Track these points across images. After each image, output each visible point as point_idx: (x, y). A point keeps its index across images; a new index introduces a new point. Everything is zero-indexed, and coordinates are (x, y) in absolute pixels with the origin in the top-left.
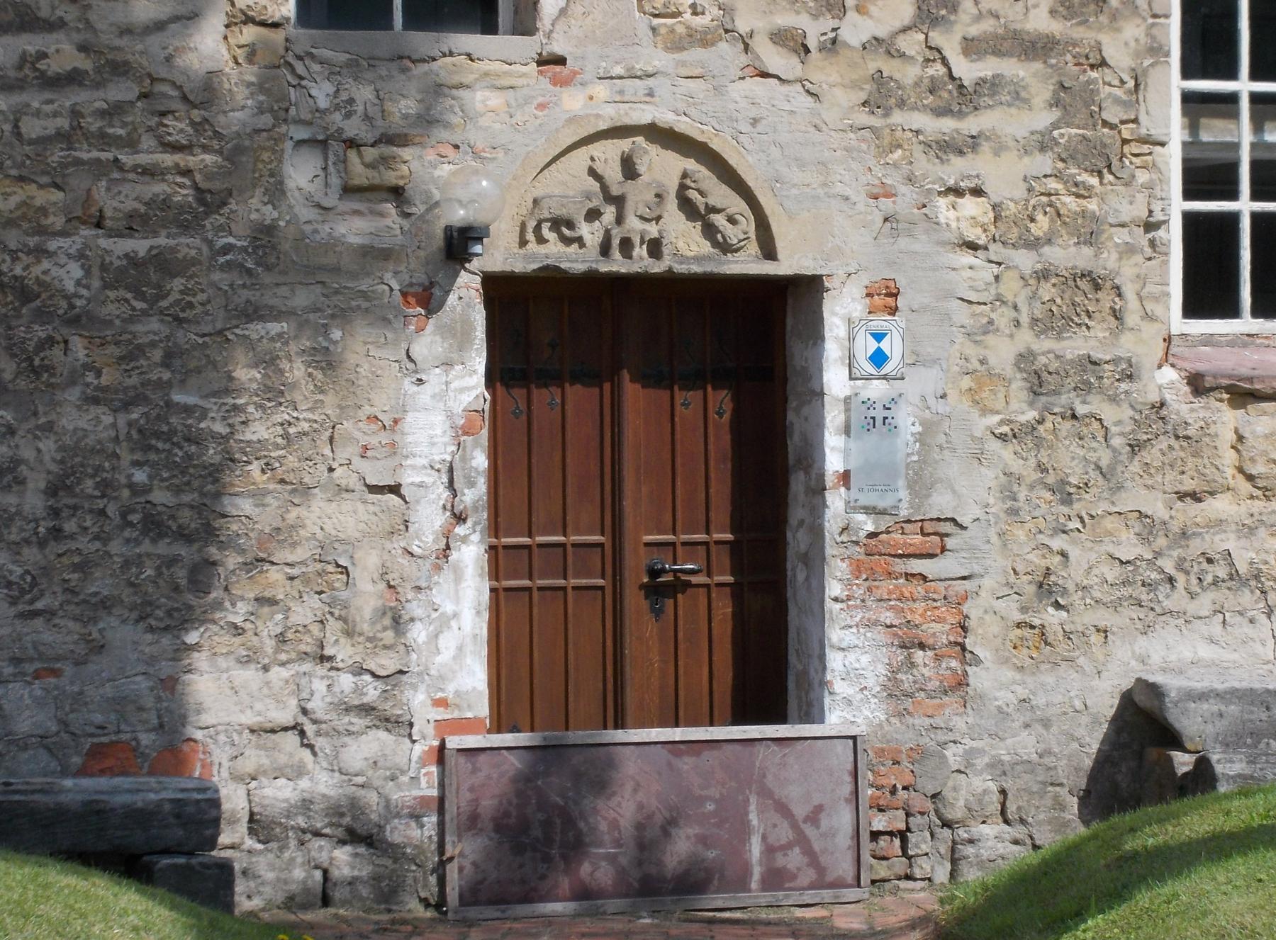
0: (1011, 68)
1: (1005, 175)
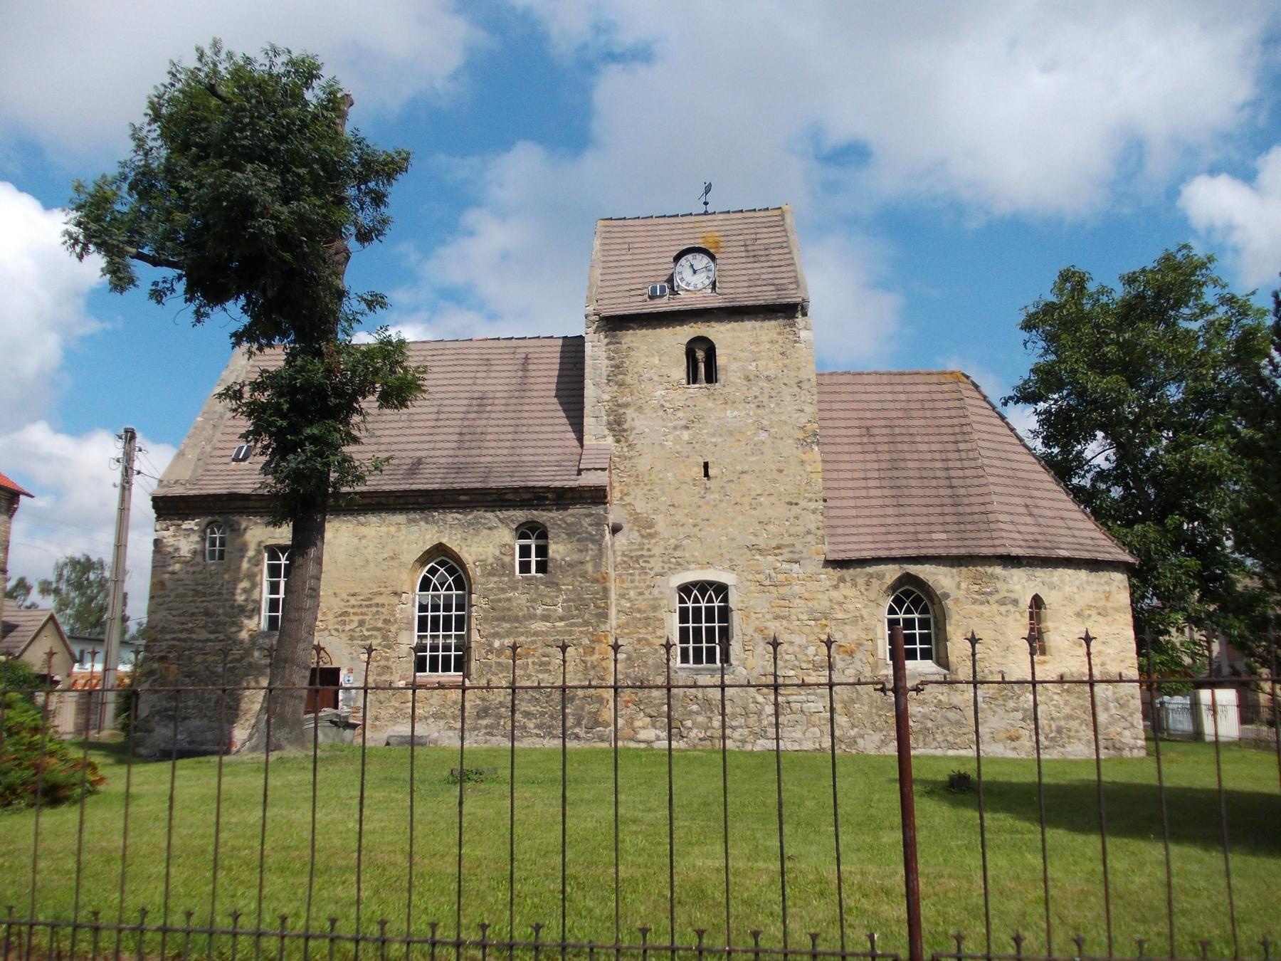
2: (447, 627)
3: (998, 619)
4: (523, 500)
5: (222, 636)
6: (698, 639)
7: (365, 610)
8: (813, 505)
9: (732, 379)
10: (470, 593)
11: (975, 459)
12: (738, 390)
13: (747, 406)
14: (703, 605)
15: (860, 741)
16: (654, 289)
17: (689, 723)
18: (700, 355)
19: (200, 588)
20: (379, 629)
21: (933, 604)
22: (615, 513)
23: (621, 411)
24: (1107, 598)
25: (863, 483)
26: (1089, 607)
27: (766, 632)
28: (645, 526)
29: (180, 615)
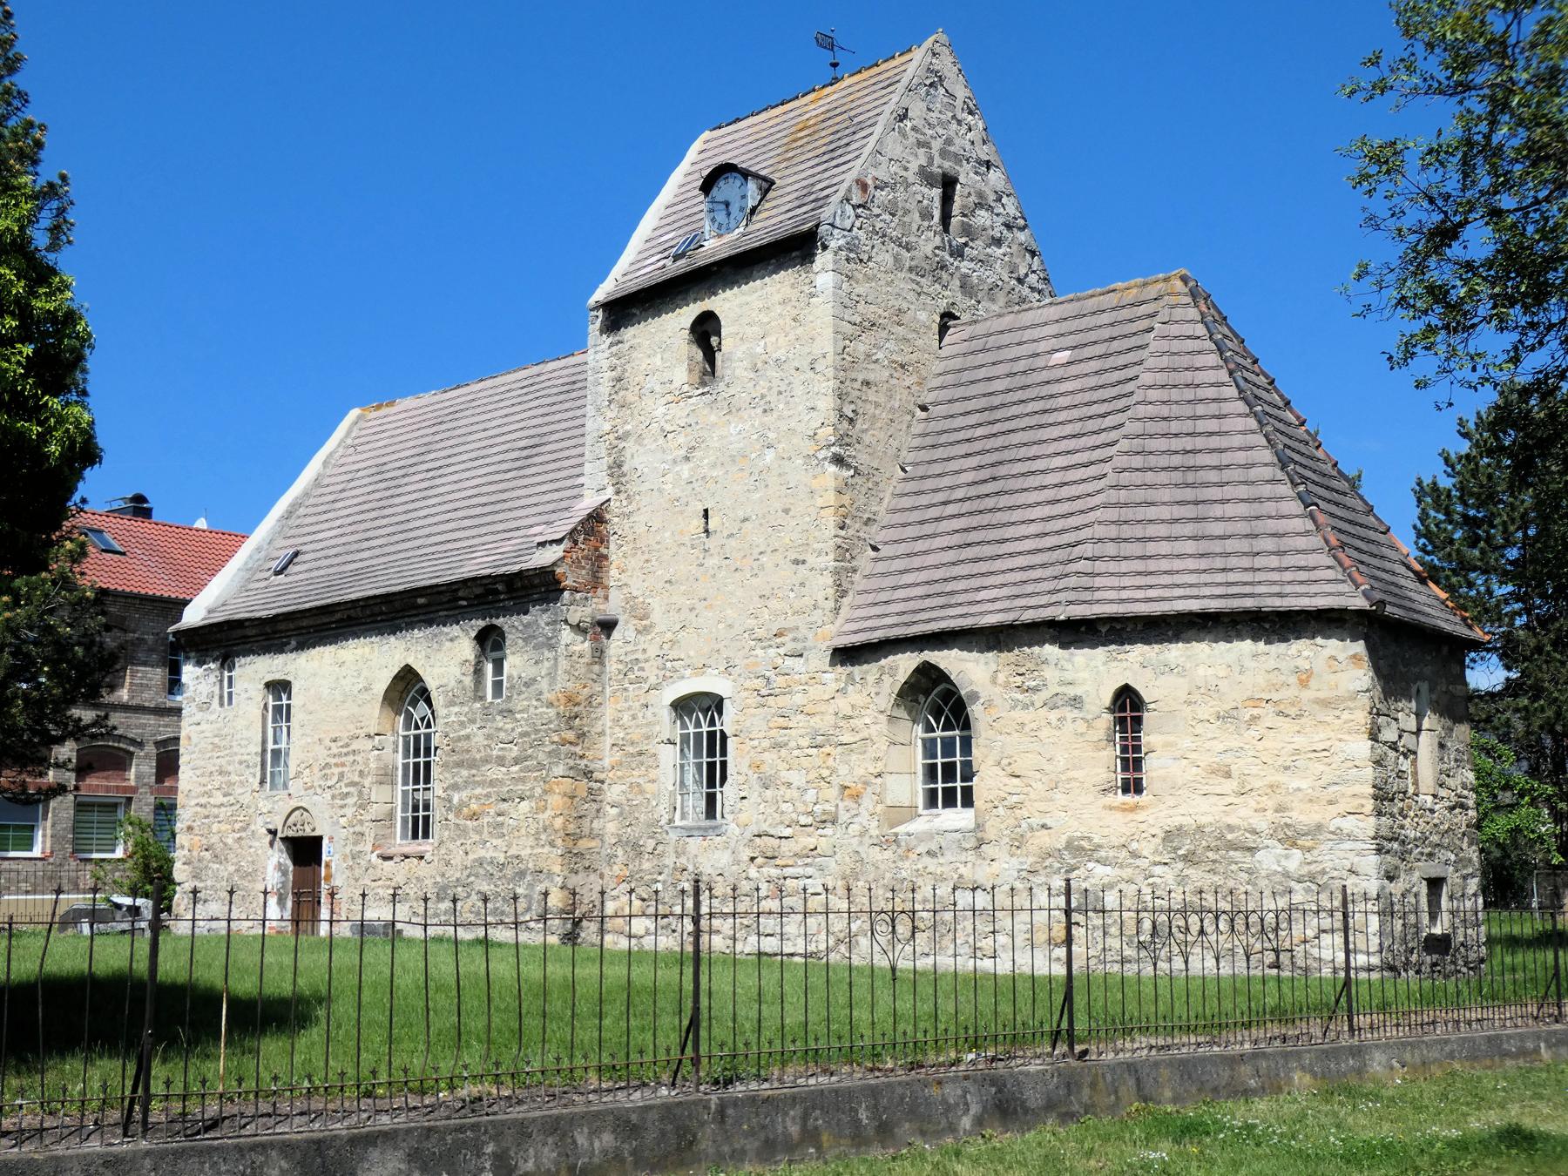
13: (753, 412)
24: (1304, 684)
26: (1255, 701)
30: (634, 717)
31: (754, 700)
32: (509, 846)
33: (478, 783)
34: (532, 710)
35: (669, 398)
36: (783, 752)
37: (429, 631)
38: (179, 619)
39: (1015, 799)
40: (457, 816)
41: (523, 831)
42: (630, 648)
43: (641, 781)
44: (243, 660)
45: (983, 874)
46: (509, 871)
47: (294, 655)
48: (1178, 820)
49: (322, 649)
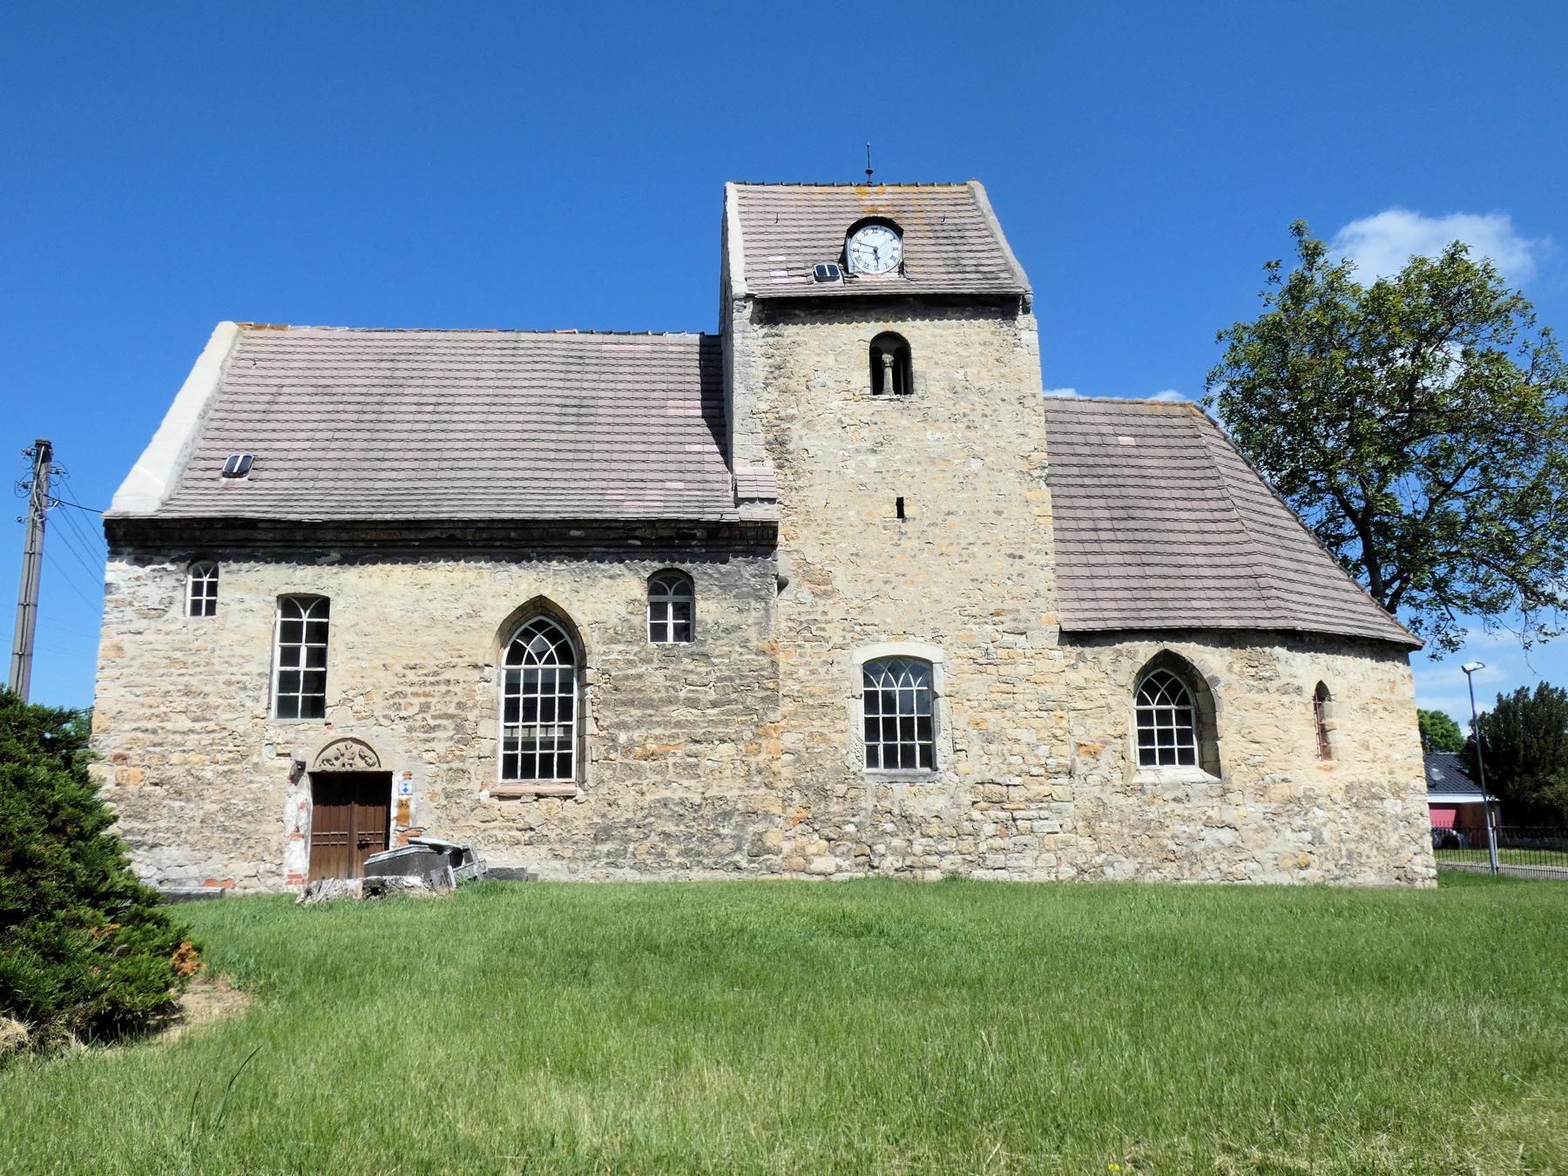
0: (444, 722)
1: (441, 747)
2: (548, 715)
3: (1279, 711)
4: (661, 538)
5: (211, 726)
6: (889, 734)
7: (428, 689)
8: (1042, 559)
9: (932, 389)
10: (583, 667)
11: (1229, 510)
12: (942, 405)
14: (897, 689)
15: (1109, 871)
16: (821, 269)
17: (881, 848)
18: (887, 358)
19: (178, 655)
20: (451, 717)
21: (1195, 690)
22: (783, 562)
23: (785, 425)
25: (1093, 536)
27: (983, 726)
28: (822, 584)
29: (147, 695)
30: (813, 672)
31: (969, 667)
32: (708, 787)
33: (659, 724)
34: (735, 656)
35: (849, 396)
36: (1008, 713)
37: (574, 565)
38: (109, 505)
39: (1257, 759)
40: (625, 755)
41: (727, 773)
42: (803, 609)
43: (825, 731)
44: (234, 566)
45: (1231, 815)
46: (707, 812)
47: (335, 568)
48: (1352, 779)
49: (388, 566)
